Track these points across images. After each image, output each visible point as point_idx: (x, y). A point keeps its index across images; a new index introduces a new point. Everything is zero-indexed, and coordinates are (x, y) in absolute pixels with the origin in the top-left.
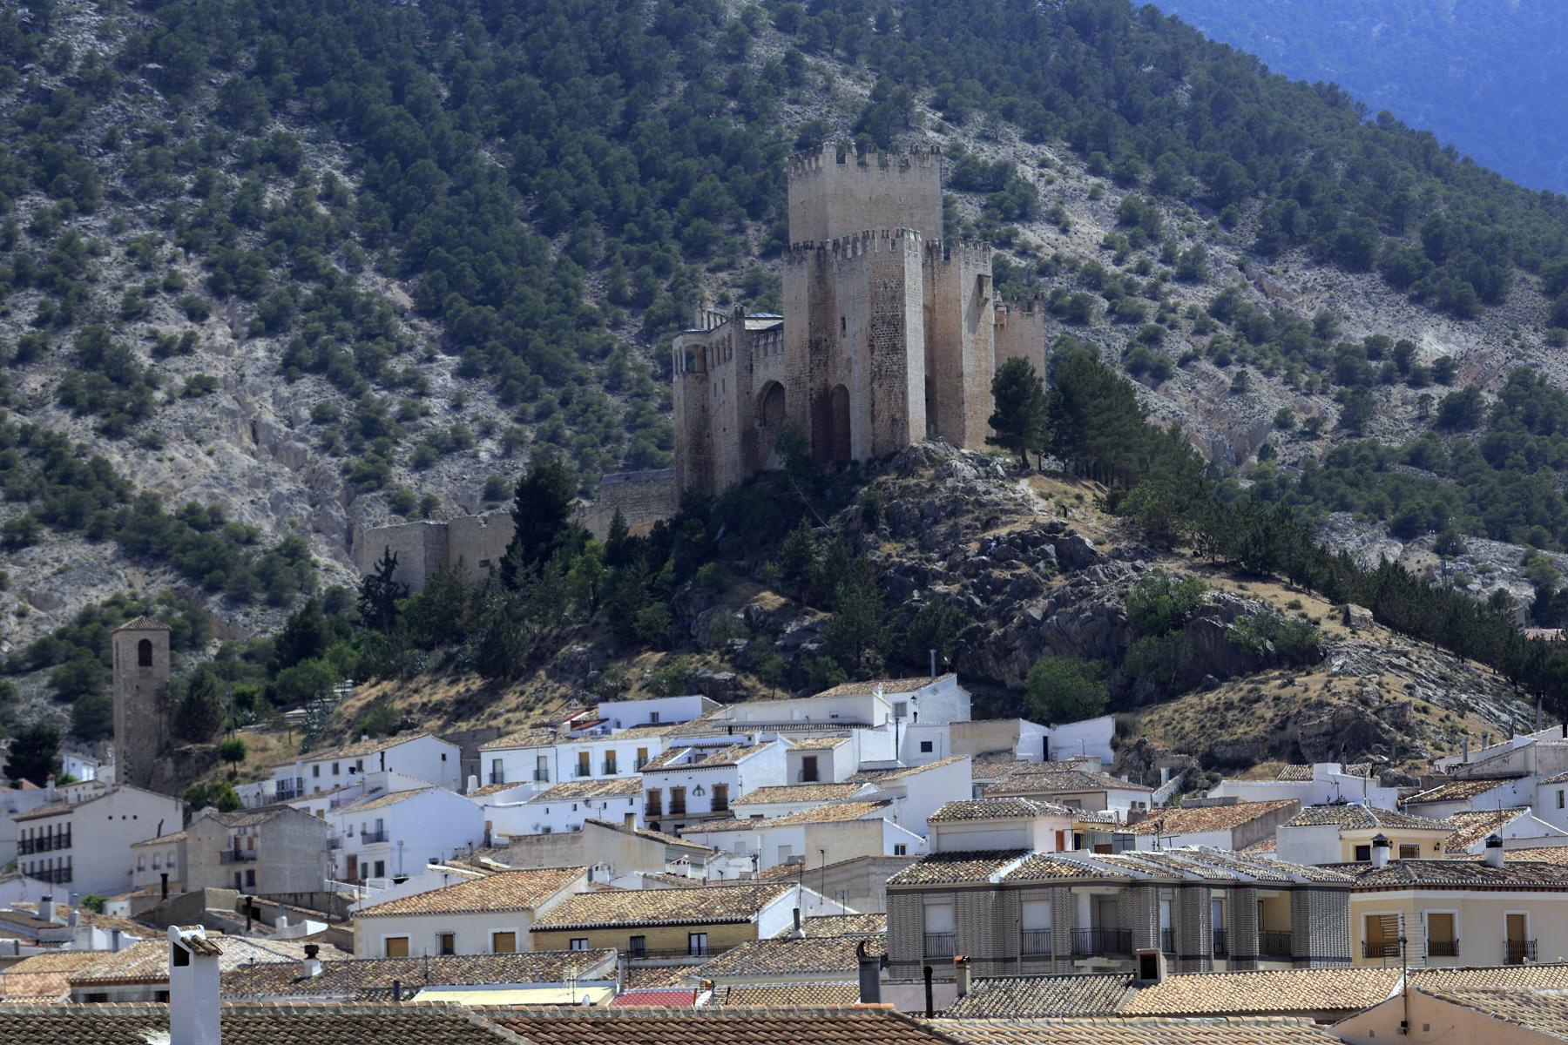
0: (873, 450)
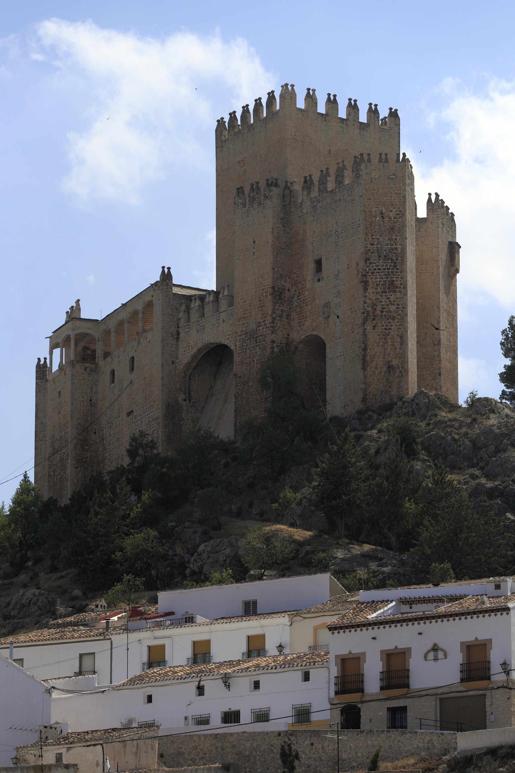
0: (364, 400)
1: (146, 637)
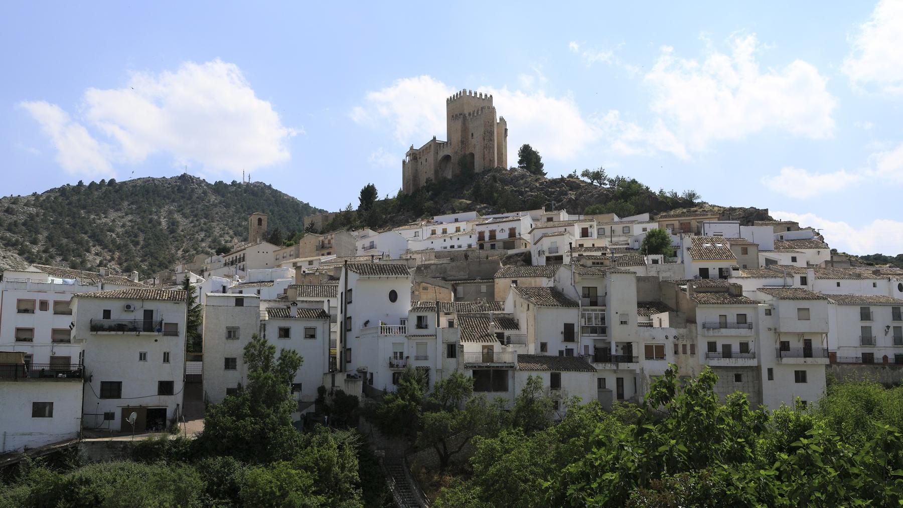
1: (432, 227)
